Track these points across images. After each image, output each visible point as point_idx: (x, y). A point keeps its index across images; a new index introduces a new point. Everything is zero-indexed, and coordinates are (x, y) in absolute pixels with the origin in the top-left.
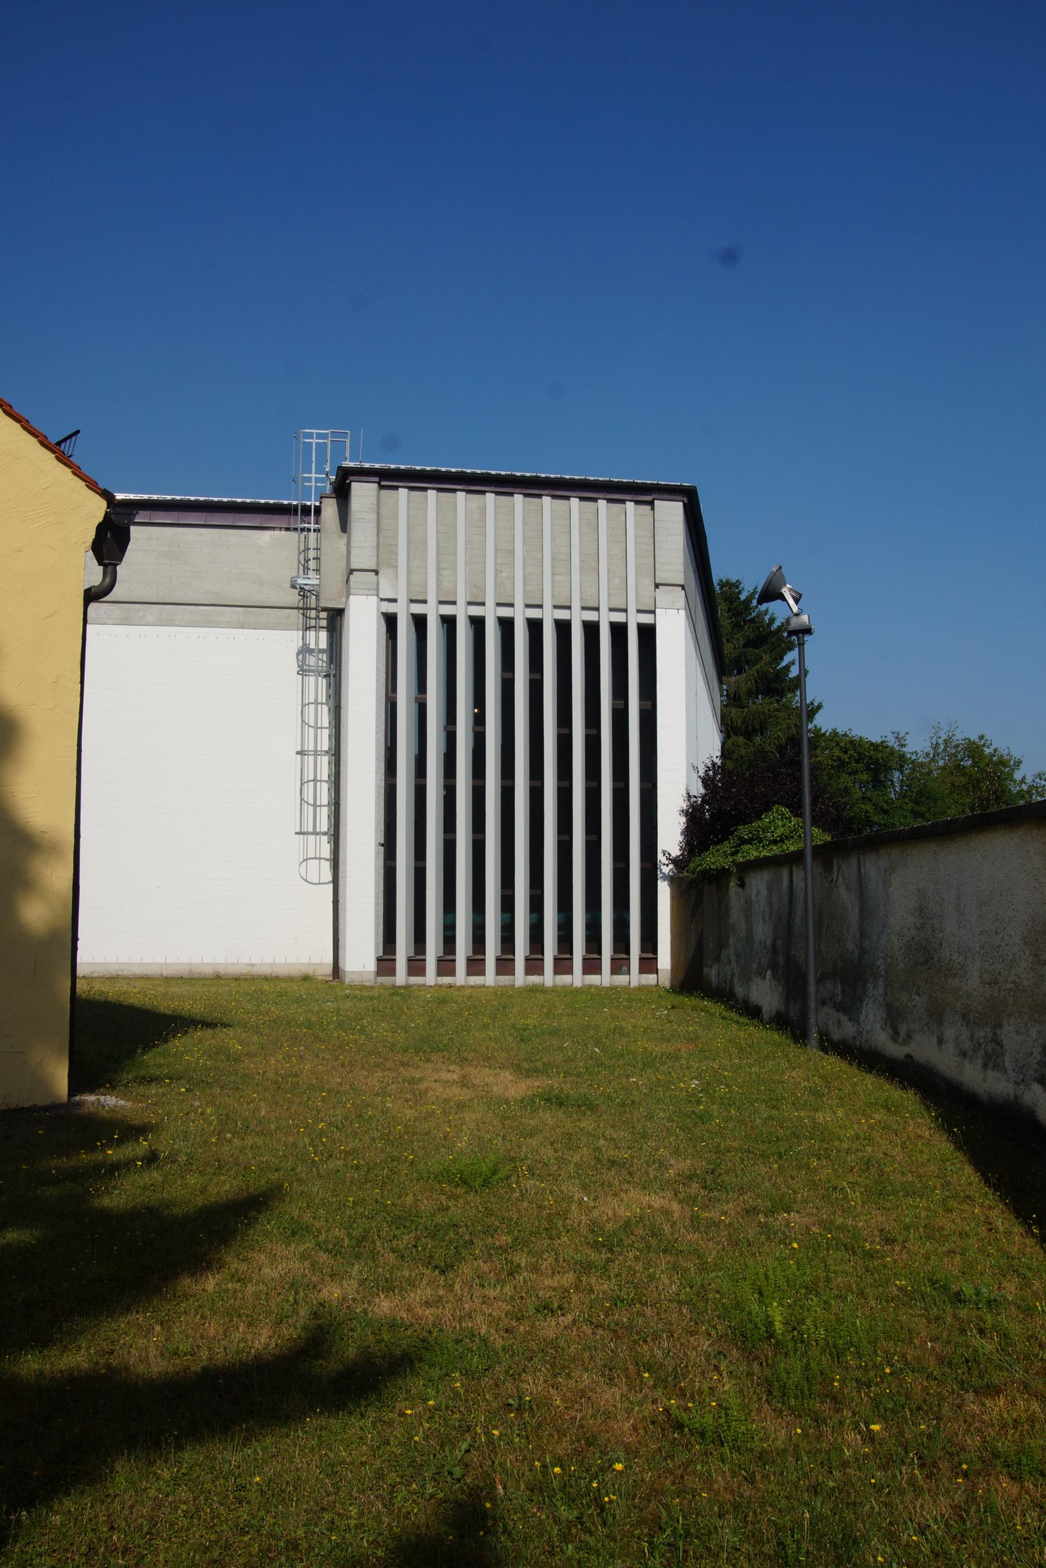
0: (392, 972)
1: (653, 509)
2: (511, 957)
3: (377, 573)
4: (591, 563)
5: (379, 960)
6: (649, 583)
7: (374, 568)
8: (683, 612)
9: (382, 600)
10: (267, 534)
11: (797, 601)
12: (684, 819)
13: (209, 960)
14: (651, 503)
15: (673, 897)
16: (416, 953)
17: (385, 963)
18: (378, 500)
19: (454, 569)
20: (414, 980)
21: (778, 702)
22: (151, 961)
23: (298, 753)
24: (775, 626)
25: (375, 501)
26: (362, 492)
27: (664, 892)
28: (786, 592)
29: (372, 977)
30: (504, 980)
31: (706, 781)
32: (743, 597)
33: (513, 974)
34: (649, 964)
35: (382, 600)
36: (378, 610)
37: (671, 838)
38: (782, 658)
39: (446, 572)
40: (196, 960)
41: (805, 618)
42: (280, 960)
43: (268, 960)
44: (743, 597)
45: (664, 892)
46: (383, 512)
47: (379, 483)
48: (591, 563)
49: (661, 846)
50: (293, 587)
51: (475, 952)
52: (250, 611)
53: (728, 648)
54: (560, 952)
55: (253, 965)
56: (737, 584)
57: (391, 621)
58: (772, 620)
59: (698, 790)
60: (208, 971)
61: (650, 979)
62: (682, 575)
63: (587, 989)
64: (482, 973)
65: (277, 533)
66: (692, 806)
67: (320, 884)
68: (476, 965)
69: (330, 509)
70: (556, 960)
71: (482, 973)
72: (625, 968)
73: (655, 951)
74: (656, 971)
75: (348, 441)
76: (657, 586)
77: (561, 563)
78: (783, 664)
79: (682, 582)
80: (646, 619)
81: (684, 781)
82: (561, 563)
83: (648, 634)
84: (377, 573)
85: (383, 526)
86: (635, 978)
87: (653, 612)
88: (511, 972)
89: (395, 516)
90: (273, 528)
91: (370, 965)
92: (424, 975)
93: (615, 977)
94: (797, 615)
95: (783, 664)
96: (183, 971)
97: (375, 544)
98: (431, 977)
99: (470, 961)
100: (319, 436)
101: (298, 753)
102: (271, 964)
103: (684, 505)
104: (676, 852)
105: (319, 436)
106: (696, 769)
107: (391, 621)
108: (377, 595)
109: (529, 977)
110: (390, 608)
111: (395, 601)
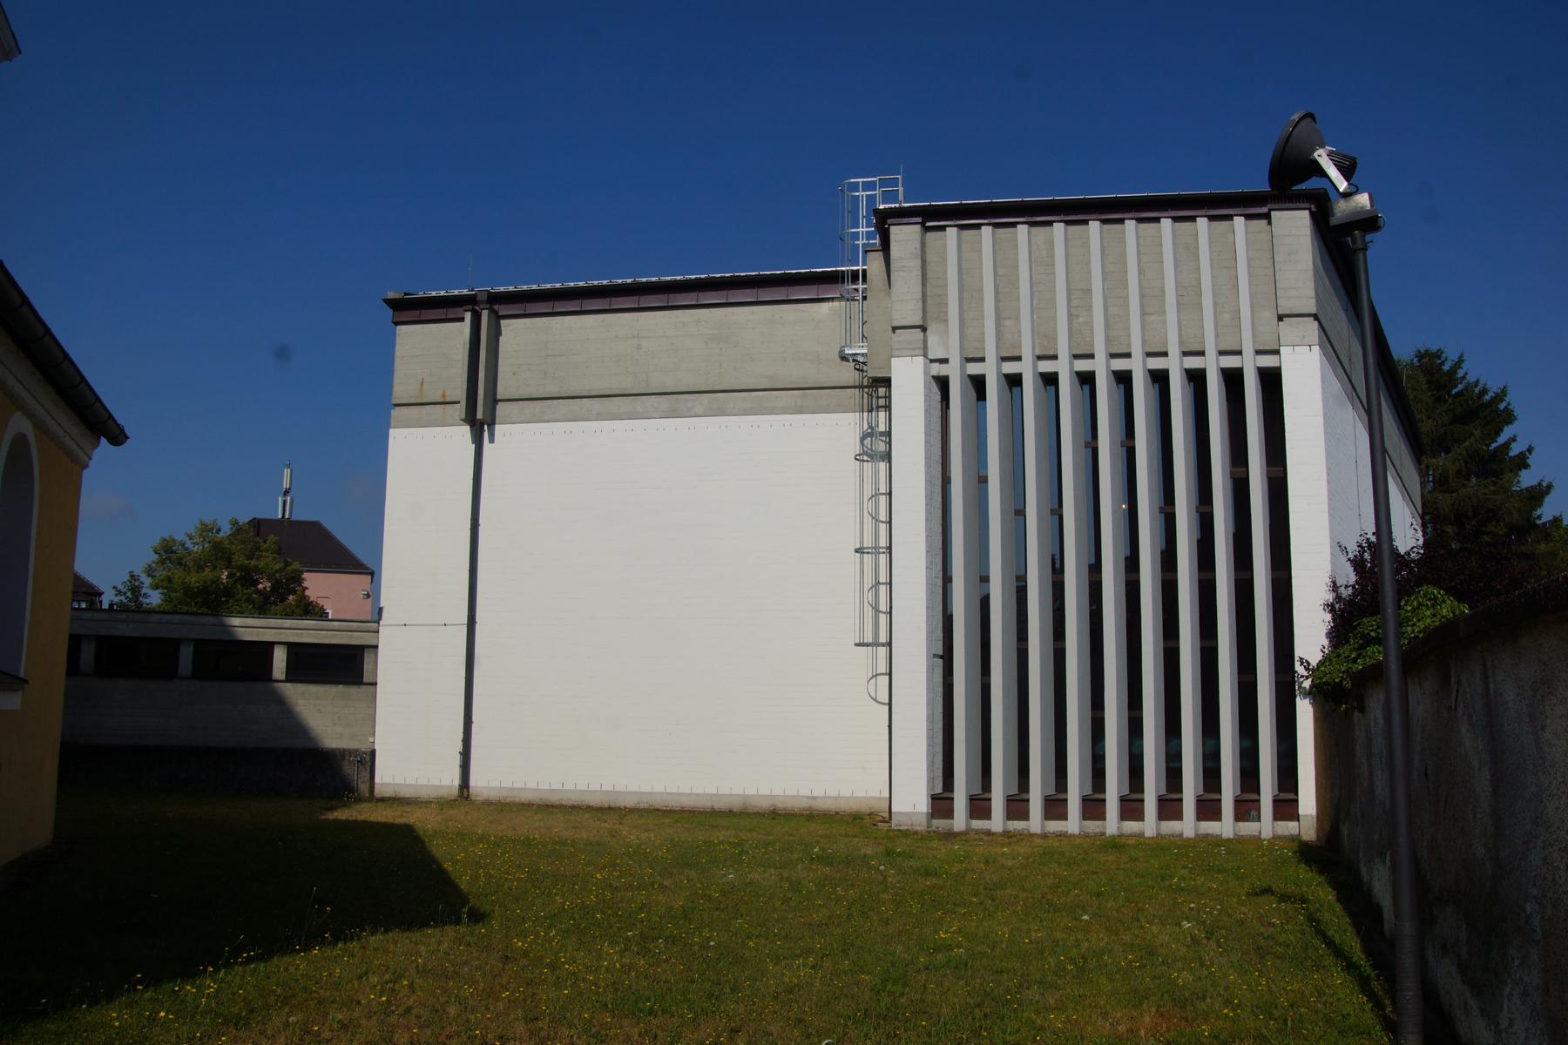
0: (948, 813)
1: (1270, 223)
2: (1253, 796)
3: (924, 329)
4: (1189, 298)
5: (934, 798)
6: (1268, 315)
7: (920, 323)
8: (1316, 349)
9: (932, 361)
10: (825, 306)
11: (1347, 172)
12: (1328, 617)
13: (764, 791)
14: (1267, 217)
15: (1318, 720)
16: (1131, 791)
17: (941, 804)
18: (923, 244)
19: (1018, 318)
20: (978, 824)
21: (1495, 484)
22: (700, 791)
23: (857, 551)
24: (1487, 397)
25: (918, 245)
26: (904, 236)
27: (1305, 712)
28: (1323, 157)
29: (924, 820)
30: (1093, 826)
31: (1357, 564)
32: (1446, 368)
33: (1104, 819)
34: (1286, 807)
35: (932, 361)
36: (926, 373)
37: (1312, 639)
38: (1498, 434)
39: (1008, 323)
40: (751, 791)
41: (1363, 200)
42: (846, 793)
43: (832, 793)
44: (1446, 368)
45: (1305, 712)
46: (929, 257)
47: (923, 224)
48: (1189, 298)
49: (1299, 652)
50: (844, 358)
51: (1169, 790)
52: (806, 394)
53: (1426, 427)
54: (1280, 790)
55: (814, 798)
56: (1439, 354)
57: (943, 383)
58: (1484, 391)
59: (1349, 576)
60: (765, 804)
61: (1289, 827)
62: (1313, 302)
63: (1239, 842)
64: (1064, 817)
65: (836, 304)
66: (1338, 598)
67: (890, 704)
68: (1055, 807)
69: (874, 265)
70: (1276, 801)
71: (1064, 817)
72: (1253, 813)
73: (1257, 789)
74: (1295, 816)
75: (901, 189)
76: (1280, 318)
77: (1151, 301)
78: (1502, 439)
79: (1313, 310)
80: (1267, 361)
81: (1329, 567)
82: (1151, 301)
83: (1271, 381)
84: (924, 329)
85: (930, 274)
86: (1266, 826)
87: (1277, 352)
88: (1101, 816)
89: (943, 261)
90: (832, 299)
91: (922, 805)
92: (989, 818)
93: (1241, 824)
94: (1346, 195)
95: (1502, 439)
96: (736, 805)
97: (919, 296)
98: (997, 821)
99: (1161, 801)
100: (867, 186)
101: (857, 551)
102: (835, 798)
103: (1312, 214)
104: (1315, 658)
105: (867, 186)
106: (1344, 550)
107: (943, 383)
108: (925, 355)
109: (1126, 823)
110: (937, 369)
111: (945, 361)
